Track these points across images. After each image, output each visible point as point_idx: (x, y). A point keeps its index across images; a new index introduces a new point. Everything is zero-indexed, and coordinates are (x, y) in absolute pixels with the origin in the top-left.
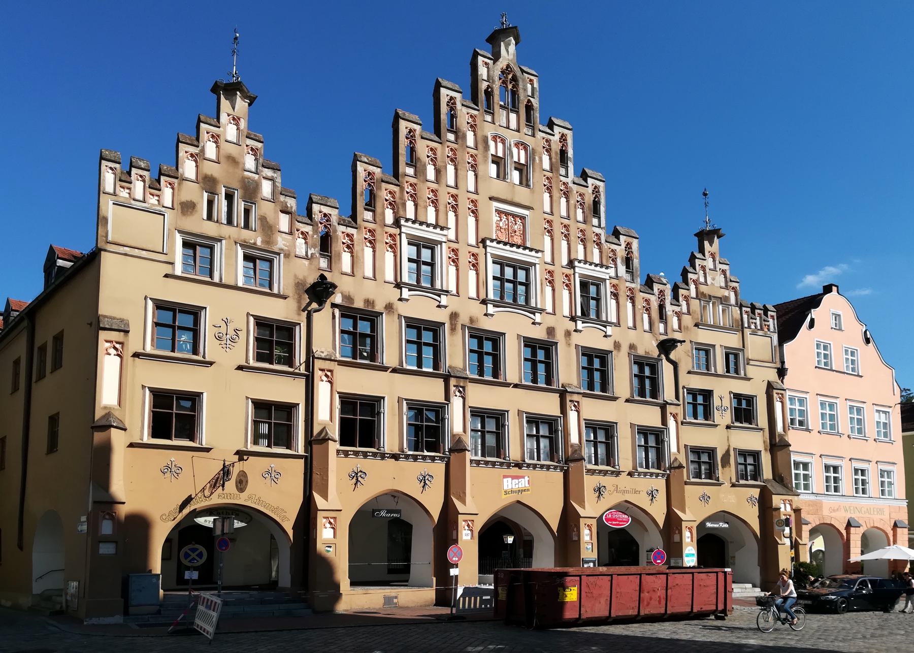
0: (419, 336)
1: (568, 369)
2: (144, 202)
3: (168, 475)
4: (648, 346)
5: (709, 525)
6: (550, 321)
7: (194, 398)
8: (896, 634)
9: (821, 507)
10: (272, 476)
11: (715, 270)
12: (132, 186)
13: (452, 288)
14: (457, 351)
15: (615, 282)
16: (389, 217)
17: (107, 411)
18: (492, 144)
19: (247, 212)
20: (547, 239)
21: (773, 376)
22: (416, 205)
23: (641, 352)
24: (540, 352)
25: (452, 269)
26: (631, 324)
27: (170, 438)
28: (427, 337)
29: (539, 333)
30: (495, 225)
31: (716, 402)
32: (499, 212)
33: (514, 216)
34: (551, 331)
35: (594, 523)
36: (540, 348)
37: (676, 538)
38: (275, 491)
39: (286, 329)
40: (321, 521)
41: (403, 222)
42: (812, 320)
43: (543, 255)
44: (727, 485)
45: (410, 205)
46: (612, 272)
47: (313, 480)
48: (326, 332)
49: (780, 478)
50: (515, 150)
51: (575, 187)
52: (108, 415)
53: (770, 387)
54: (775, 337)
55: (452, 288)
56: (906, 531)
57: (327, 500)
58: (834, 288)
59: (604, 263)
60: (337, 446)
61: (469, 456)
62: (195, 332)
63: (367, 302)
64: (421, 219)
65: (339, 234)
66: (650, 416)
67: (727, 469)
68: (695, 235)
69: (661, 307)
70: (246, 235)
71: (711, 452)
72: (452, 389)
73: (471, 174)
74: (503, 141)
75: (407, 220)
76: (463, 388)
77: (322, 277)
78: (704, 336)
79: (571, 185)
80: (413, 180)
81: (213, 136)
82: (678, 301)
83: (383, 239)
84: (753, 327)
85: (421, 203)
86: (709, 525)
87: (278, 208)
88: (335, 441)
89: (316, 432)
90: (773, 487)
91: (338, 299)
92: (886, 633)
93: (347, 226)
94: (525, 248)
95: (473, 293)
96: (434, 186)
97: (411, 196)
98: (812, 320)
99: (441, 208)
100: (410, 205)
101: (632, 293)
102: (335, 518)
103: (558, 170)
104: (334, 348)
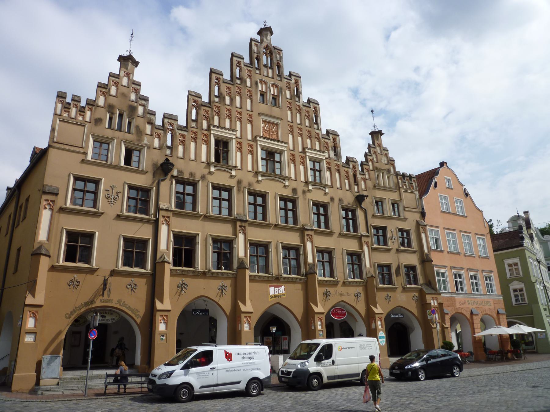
0: (255, 200)
1: (306, 215)
2: (75, 119)
3: (71, 287)
4: (349, 199)
5: (392, 316)
6: (294, 185)
7: (90, 236)
8: (493, 390)
9: (455, 301)
10: (132, 287)
11: (381, 154)
12: (70, 110)
13: (239, 165)
14: (242, 205)
15: (328, 161)
16: (205, 124)
17: (40, 244)
18: (259, 85)
19: (130, 123)
20: (290, 136)
21: (417, 217)
22: (219, 118)
23: (346, 203)
24: (289, 202)
25: (239, 154)
26: (339, 186)
27: (74, 261)
28: (259, 200)
29: (287, 193)
30: (262, 129)
31: (389, 234)
32: (264, 121)
33: (273, 124)
34: (294, 191)
35: (323, 317)
36: (321, 207)
37: (373, 326)
38: (129, 298)
39: (146, 191)
40: (158, 318)
41: (212, 128)
42: (436, 183)
43: (289, 145)
44: (400, 289)
45: (216, 118)
46: (326, 155)
47: (154, 291)
48: (167, 194)
49: (430, 284)
50: (272, 88)
51: (304, 108)
52: (40, 247)
53: (418, 224)
54: (417, 193)
55: (239, 165)
56: (505, 317)
57: (163, 303)
58: (445, 164)
59: (322, 150)
60: (171, 267)
61: (248, 273)
62: (96, 193)
63: (192, 174)
64: (222, 125)
65: (178, 134)
66: (353, 245)
67: (399, 277)
68: (370, 134)
69: (355, 176)
70: (129, 137)
71: (389, 267)
72: (238, 228)
73: (249, 101)
74: (265, 83)
75: (214, 126)
76: (245, 227)
77: (167, 160)
78: (380, 194)
79: (301, 106)
80: (218, 105)
81: (115, 83)
82: (363, 172)
83: (201, 137)
84: (405, 187)
85: (222, 116)
86: (392, 316)
87: (146, 121)
88: (169, 263)
89: (158, 257)
90: (426, 289)
91: (175, 173)
92: (487, 389)
93: (182, 130)
94: (279, 141)
95: (250, 168)
96: (229, 107)
97: (217, 113)
98: (436, 183)
99: (233, 119)
100: (216, 118)
101: (338, 167)
102: (166, 316)
103: (295, 98)
104: (170, 202)
